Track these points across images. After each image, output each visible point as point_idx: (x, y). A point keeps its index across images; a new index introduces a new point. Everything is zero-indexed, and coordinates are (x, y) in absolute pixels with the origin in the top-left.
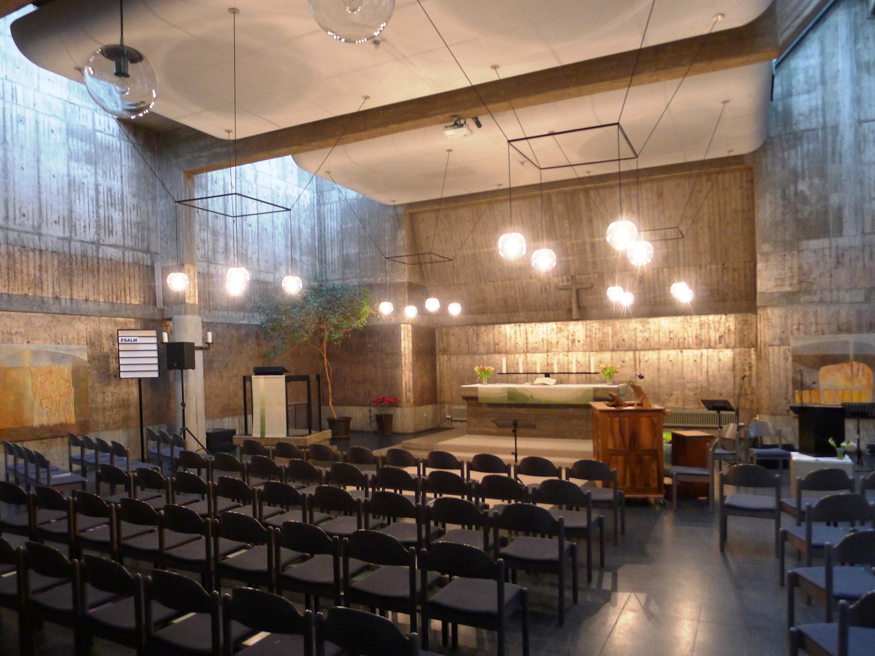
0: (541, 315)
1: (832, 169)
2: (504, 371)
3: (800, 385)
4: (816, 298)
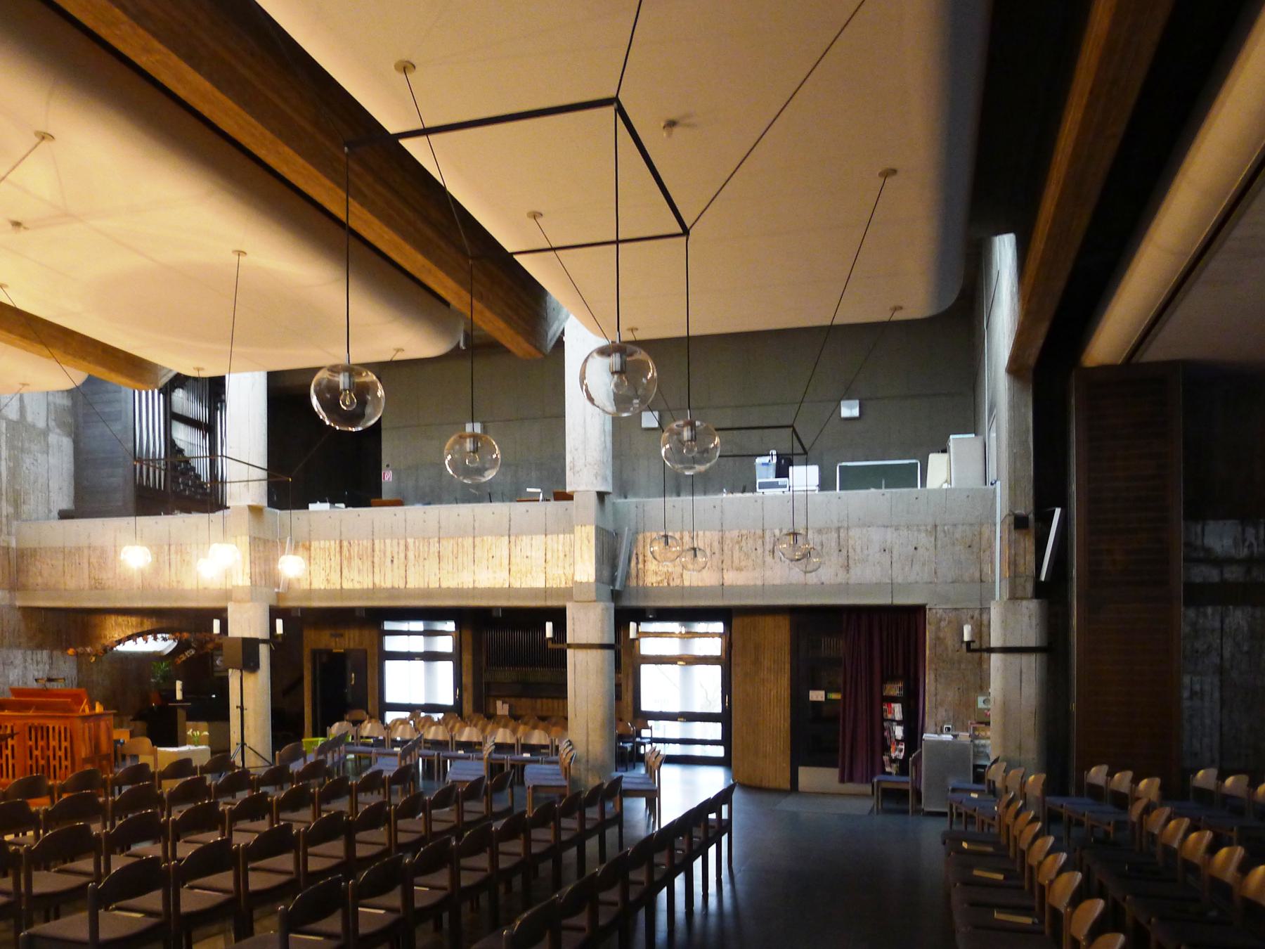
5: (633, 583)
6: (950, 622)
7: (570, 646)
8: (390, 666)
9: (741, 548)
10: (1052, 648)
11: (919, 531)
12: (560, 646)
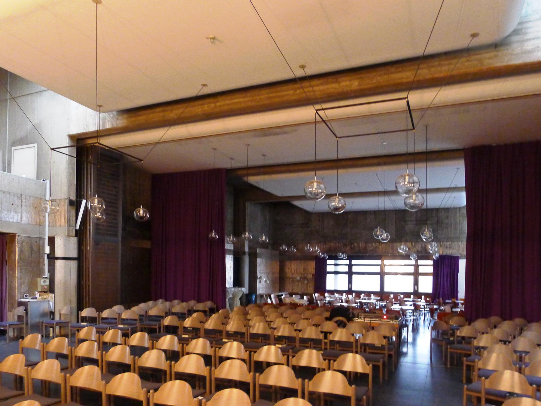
6: (27, 243)
10: (80, 259)
11: (14, 196)
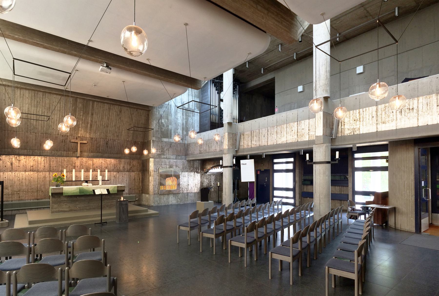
0: (106, 155)
1: (169, 118)
2: (74, 180)
3: (161, 184)
4: (165, 157)
5: (340, 135)
7: (328, 162)
8: (276, 175)
9: (386, 113)
12: (311, 163)
